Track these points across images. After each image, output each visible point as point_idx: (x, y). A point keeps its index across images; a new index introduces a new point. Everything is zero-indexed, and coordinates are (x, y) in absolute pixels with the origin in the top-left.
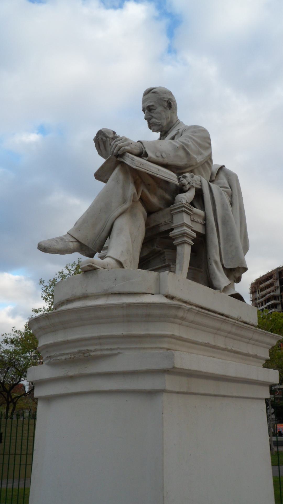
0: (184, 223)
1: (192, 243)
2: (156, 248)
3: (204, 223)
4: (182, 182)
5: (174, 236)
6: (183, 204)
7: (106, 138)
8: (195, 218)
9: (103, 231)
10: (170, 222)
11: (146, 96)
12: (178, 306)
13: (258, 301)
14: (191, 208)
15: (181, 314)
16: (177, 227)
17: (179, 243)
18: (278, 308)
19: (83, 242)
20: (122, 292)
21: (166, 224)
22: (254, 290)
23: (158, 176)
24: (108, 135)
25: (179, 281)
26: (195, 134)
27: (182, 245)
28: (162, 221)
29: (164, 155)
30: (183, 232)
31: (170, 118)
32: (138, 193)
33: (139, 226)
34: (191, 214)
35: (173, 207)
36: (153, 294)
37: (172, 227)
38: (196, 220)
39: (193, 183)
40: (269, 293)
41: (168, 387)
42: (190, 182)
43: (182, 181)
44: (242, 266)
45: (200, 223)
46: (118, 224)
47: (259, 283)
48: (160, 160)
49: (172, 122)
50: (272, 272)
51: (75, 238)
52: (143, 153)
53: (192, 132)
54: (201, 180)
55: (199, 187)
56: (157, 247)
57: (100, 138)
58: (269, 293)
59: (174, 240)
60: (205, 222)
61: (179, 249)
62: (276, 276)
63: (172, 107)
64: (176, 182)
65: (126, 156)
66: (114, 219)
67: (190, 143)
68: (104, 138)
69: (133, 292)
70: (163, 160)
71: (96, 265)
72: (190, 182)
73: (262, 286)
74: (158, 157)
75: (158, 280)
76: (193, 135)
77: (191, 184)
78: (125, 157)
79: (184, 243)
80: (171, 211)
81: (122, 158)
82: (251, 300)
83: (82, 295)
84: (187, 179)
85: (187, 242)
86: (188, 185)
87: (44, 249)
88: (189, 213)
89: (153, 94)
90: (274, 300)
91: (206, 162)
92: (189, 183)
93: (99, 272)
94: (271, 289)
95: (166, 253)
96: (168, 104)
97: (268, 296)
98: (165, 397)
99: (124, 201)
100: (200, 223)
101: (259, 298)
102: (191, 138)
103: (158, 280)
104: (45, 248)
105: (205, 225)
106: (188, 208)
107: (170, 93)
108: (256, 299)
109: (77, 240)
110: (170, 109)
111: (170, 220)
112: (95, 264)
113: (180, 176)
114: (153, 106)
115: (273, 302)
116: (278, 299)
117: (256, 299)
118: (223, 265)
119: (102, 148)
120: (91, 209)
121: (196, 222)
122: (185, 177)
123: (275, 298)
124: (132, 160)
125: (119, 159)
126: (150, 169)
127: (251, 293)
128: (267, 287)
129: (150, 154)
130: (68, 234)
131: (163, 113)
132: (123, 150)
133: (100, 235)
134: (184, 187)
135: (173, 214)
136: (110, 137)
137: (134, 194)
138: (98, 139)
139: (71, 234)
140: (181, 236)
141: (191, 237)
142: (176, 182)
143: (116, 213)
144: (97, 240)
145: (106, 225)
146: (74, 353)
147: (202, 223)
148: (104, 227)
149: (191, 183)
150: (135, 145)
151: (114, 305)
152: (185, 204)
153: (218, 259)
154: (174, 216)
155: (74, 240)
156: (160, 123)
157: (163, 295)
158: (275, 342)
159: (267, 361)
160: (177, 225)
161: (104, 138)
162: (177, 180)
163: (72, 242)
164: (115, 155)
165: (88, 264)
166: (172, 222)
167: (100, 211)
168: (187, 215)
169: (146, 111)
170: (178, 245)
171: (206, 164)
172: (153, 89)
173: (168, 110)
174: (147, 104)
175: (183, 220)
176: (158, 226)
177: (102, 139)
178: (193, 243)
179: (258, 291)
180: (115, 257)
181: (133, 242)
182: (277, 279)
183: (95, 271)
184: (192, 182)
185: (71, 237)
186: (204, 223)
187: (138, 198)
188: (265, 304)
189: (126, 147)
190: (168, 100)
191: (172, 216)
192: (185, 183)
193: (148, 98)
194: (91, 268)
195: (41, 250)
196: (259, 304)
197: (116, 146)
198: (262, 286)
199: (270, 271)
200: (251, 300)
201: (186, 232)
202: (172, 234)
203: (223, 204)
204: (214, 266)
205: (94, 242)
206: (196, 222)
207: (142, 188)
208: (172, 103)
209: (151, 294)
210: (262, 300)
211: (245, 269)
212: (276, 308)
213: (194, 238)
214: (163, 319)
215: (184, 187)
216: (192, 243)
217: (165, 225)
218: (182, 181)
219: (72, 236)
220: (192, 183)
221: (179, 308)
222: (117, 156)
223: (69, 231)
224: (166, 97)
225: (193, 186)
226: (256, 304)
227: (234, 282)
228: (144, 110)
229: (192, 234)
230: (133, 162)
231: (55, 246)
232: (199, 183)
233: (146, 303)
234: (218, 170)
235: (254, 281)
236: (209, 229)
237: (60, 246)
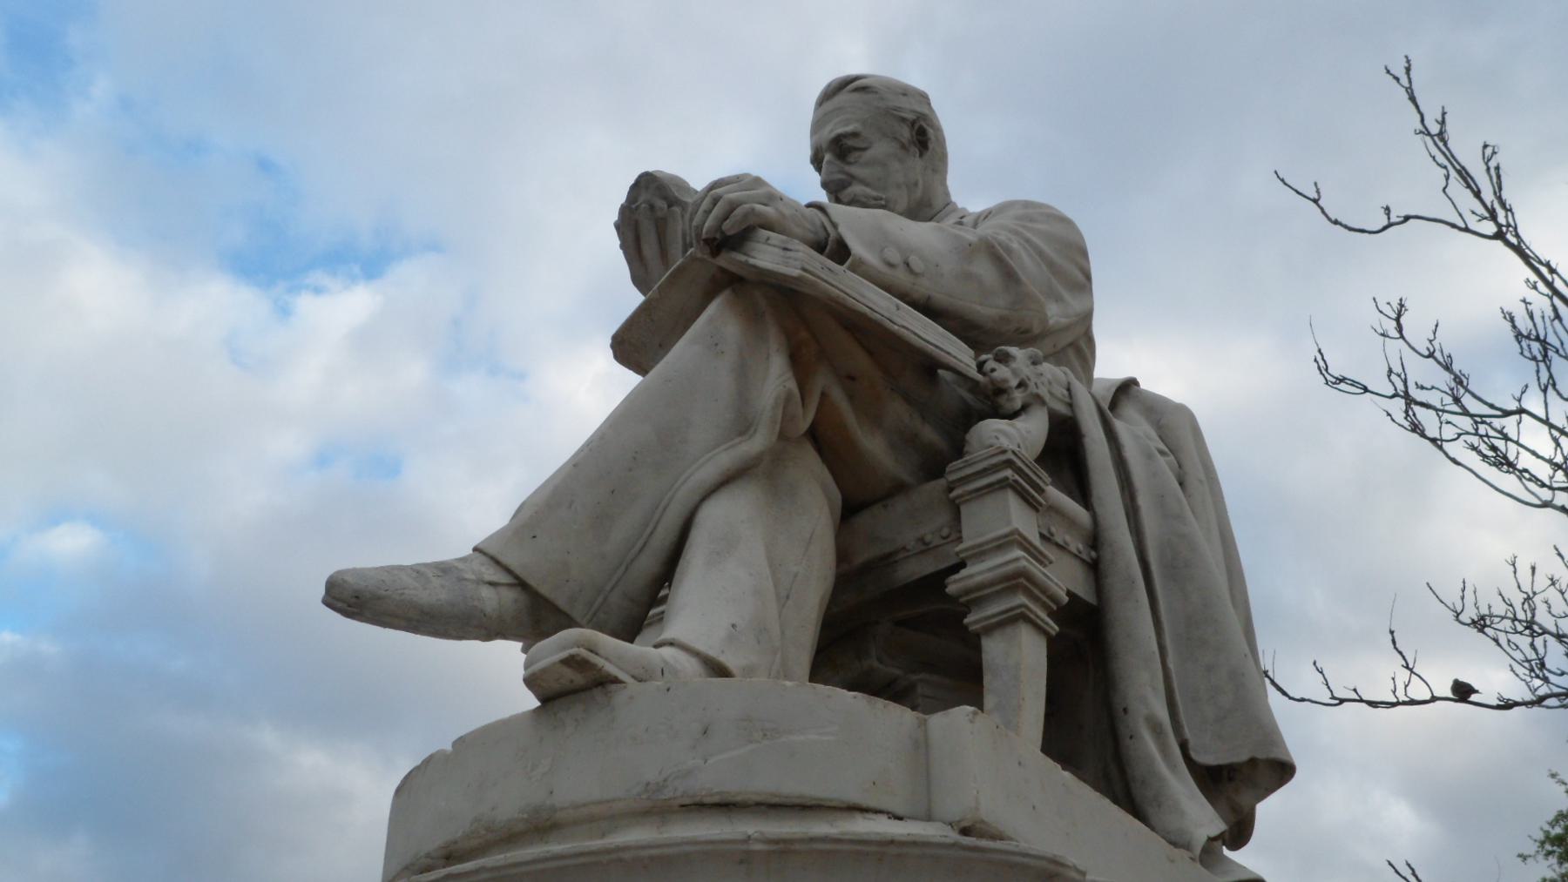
0: (1017, 532)
1: (1052, 628)
2: (876, 664)
3: (1092, 559)
4: (995, 374)
5: (968, 591)
6: (1004, 452)
7: (670, 206)
8: (1053, 530)
9: (641, 550)
10: (944, 538)
11: (829, 106)
12: (1044, 864)
14: (1041, 478)
16: (980, 553)
17: (994, 620)
19: (544, 590)
20: (738, 798)
21: (926, 548)
23: (896, 327)
24: (676, 194)
25: (1020, 763)
26: (1030, 225)
27: (1009, 630)
28: (908, 537)
29: (914, 260)
30: (1011, 567)
31: (920, 183)
32: (803, 399)
33: (811, 538)
34: (1041, 504)
35: (961, 469)
36: (900, 818)
37: (957, 554)
38: (1058, 539)
39: (1040, 385)
42: (1029, 379)
43: (993, 370)
44: (1272, 755)
45: (1076, 556)
46: (713, 516)
48: (901, 277)
49: (930, 206)
51: (508, 570)
52: (829, 243)
53: (1019, 218)
54: (1069, 383)
55: (1061, 408)
56: (880, 661)
57: (644, 202)
59: (967, 608)
60: (1093, 554)
61: (993, 649)
63: (931, 146)
64: (971, 370)
65: (759, 242)
66: (697, 498)
67: (1015, 246)
68: (661, 204)
69: (798, 801)
70: (914, 284)
71: (606, 659)
72: (1028, 382)
74: (891, 265)
75: (921, 746)
76: (1024, 227)
77: (1032, 388)
78: (751, 245)
79: (1018, 617)
80: (951, 490)
81: (740, 252)
83: (525, 816)
84: (1014, 365)
85: (1032, 616)
86: (1020, 390)
87: (354, 600)
88: (1029, 498)
89: (856, 96)
91: (1071, 345)
92: (1022, 385)
93: (620, 697)
95: (919, 690)
96: (914, 133)
99: (743, 426)
100: (1076, 556)
102: (1016, 233)
103: (921, 746)
104: (357, 597)
105: (1095, 568)
106: (1027, 475)
107: (923, 98)
109: (516, 577)
110: (921, 155)
111: (945, 532)
112: (601, 652)
113: (984, 357)
114: (855, 135)
118: (1184, 746)
119: (650, 249)
120: (591, 450)
121: (1057, 545)
122: (1004, 359)
124: (786, 249)
125: (727, 260)
126: (864, 296)
130: (477, 554)
131: (896, 165)
132: (746, 216)
133: (627, 569)
134: (1002, 400)
135: (957, 501)
136: (686, 203)
137: (788, 398)
138: (637, 208)
139: (492, 551)
140: (1003, 590)
141: (1045, 599)
142: (971, 370)
143: (708, 471)
144: (612, 589)
145: (658, 522)
147: (1084, 556)
148: (649, 530)
149: (1031, 385)
150: (796, 211)
151: (698, 848)
152: (1014, 452)
153: (1163, 714)
154: (963, 509)
155: (503, 578)
156: (881, 199)
157: (951, 824)
160: (980, 545)
161: (661, 204)
162: (973, 365)
163: (492, 584)
164: (706, 241)
165: (564, 654)
166: (953, 537)
167: (635, 458)
168: (1024, 505)
170: (989, 630)
171: (1071, 353)
172: (857, 78)
173: (915, 156)
174: (832, 131)
175: (1009, 523)
176: (887, 560)
177: (652, 207)
178: (1057, 628)
180: (701, 646)
181: (783, 599)
183: (597, 692)
184: (1034, 379)
185: (492, 563)
186: (1092, 559)
187: (804, 425)
189: (759, 207)
190: (915, 117)
191: (956, 510)
192: (1005, 381)
193: (839, 110)
194: (579, 679)
195: (340, 605)
197: (715, 201)
201: (1024, 567)
202: (955, 581)
203: (1163, 496)
205: (600, 599)
206: (1057, 545)
207: (823, 380)
208: (930, 131)
209: (888, 813)
211: (1282, 771)
213: (1058, 608)
215: (1002, 400)
216: (1054, 628)
217: (922, 552)
218: (993, 370)
219: (497, 562)
220: (1037, 387)
222: (721, 243)
223: (482, 542)
224: (909, 106)
225: (1039, 399)
227: (1224, 844)
228: (817, 161)
229: (1049, 582)
230: (790, 258)
231: (406, 591)
232: (1063, 395)
233: (873, 837)
234: (1114, 390)
236: (1115, 584)
237: (437, 594)
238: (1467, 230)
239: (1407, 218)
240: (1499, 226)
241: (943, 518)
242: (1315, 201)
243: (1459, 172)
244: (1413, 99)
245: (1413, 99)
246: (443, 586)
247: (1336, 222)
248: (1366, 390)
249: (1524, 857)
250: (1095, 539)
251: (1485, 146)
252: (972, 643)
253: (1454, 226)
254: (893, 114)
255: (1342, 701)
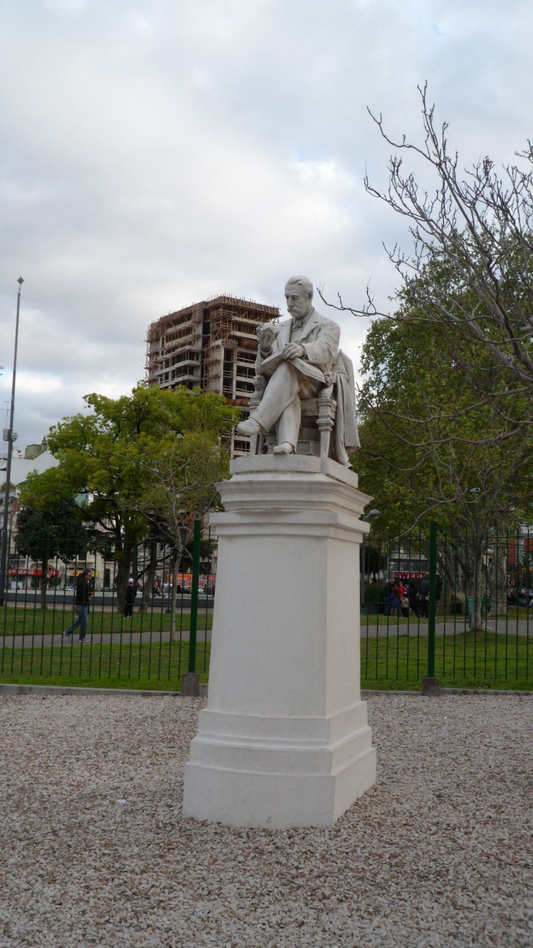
13: (160, 358)
15: (339, 489)
16: (322, 417)
18: (195, 373)
22: (154, 337)
40: (183, 345)
41: (331, 535)
47: (165, 324)
48: (315, 362)
50: (192, 307)
58: (183, 345)
61: (323, 434)
62: (198, 316)
73: (170, 330)
79: (327, 430)
82: (148, 355)
90: (190, 359)
94: (187, 338)
97: (179, 350)
98: (329, 541)
99: (291, 395)
101: (163, 352)
108: (157, 353)
115: (187, 362)
116: (197, 359)
117: (157, 353)
123: (192, 355)
127: (148, 341)
128: (180, 334)
129: (310, 358)
146: (267, 509)
158: (367, 502)
159: (362, 515)
169: (290, 299)
179: (163, 338)
182: (199, 323)
188: (173, 365)
196: (161, 363)
198: (170, 330)
199: (189, 305)
200: (148, 355)
204: (340, 445)
207: (302, 385)
210: (168, 356)
212: (191, 373)
214: (329, 491)
221: (339, 485)
224: (308, 289)
226: (157, 363)
235: (157, 321)
236: (339, 416)
238: (429, 159)
239: (410, 146)
240: (440, 160)
241: (314, 407)
242: (379, 124)
243: (432, 136)
244: (424, 101)
245: (424, 101)
246: (217, 392)
247: (385, 136)
248: (380, 196)
249: (391, 298)
250: (337, 408)
251: (445, 124)
252: (319, 432)
253: (425, 156)
254: (305, 292)
255: (345, 309)
